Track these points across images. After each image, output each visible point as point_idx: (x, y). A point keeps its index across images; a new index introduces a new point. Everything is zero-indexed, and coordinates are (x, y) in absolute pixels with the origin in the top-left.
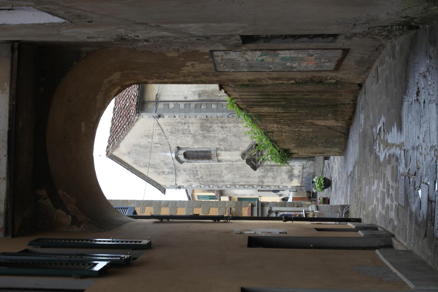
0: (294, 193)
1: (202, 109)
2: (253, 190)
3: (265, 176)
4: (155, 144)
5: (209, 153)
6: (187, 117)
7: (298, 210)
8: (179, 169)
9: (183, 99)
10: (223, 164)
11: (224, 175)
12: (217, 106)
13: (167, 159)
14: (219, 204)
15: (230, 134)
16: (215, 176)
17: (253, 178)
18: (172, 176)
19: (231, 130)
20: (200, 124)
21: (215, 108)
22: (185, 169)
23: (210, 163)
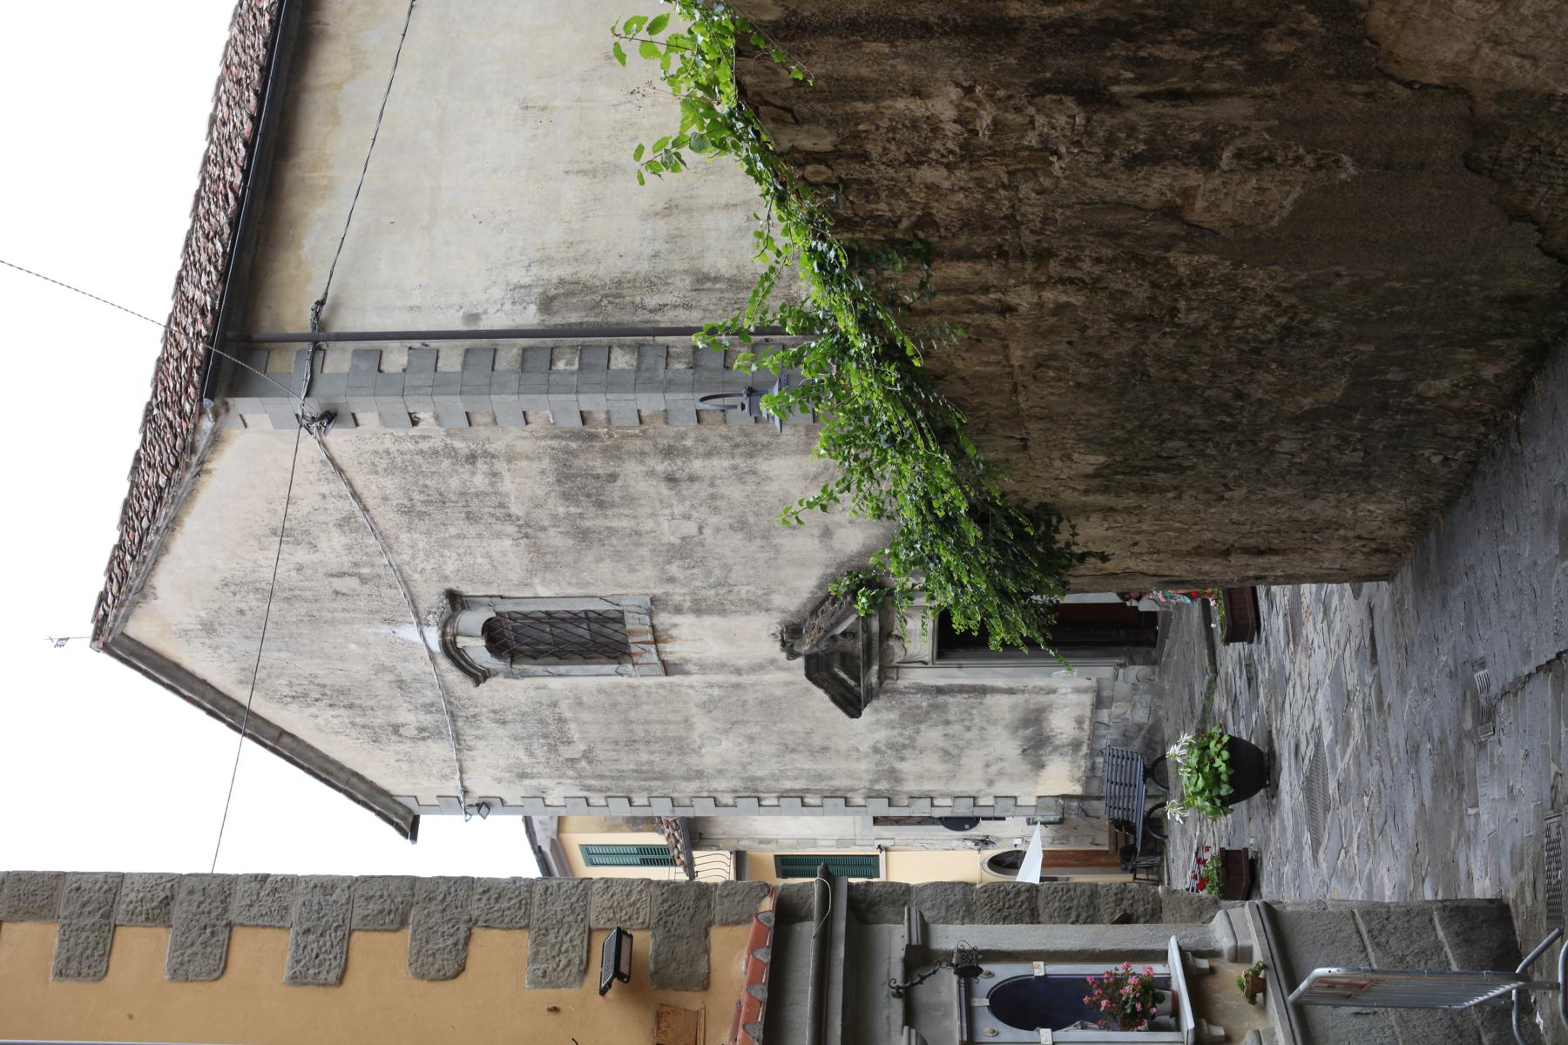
0: (1049, 831)
1: (558, 372)
2: (849, 819)
3: (904, 747)
4: (332, 576)
5: (617, 626)
6: (477, 418)
7: (1129, 946)
8: (472, 711)
9: (459, 326)
10: (691, 687)
11: (698, 741)
12: (640, 358)
13: (405, 660)
14: (537, 898)
15: (714, 520)
16: (657, 747)
17: (847, 757)
18: (441, 750)
19: (722, 497)
20: (553, 458)
21: (626, 366)
22: (503, 711)
23: (625, 680)
